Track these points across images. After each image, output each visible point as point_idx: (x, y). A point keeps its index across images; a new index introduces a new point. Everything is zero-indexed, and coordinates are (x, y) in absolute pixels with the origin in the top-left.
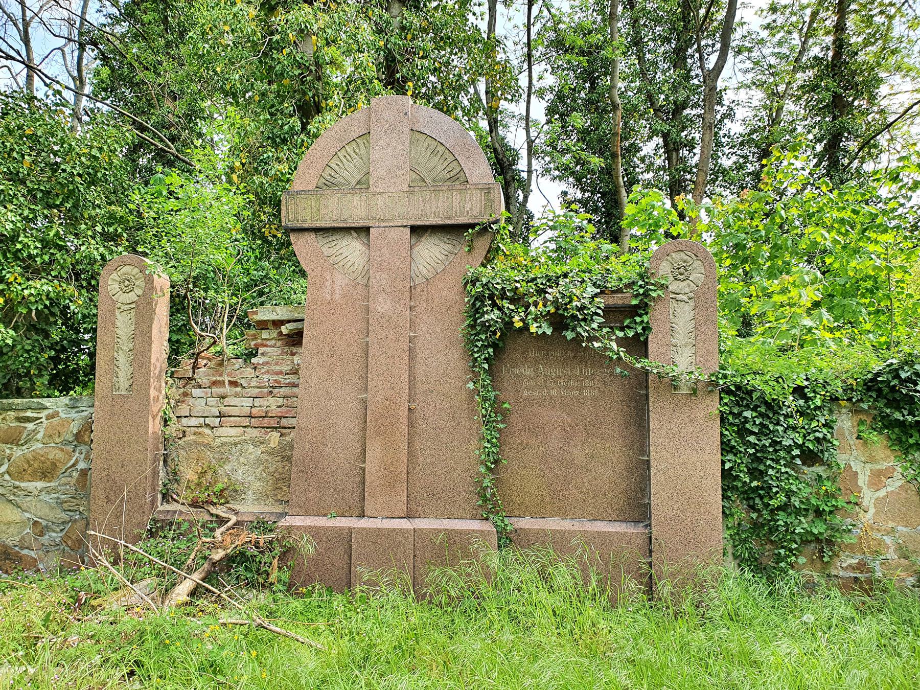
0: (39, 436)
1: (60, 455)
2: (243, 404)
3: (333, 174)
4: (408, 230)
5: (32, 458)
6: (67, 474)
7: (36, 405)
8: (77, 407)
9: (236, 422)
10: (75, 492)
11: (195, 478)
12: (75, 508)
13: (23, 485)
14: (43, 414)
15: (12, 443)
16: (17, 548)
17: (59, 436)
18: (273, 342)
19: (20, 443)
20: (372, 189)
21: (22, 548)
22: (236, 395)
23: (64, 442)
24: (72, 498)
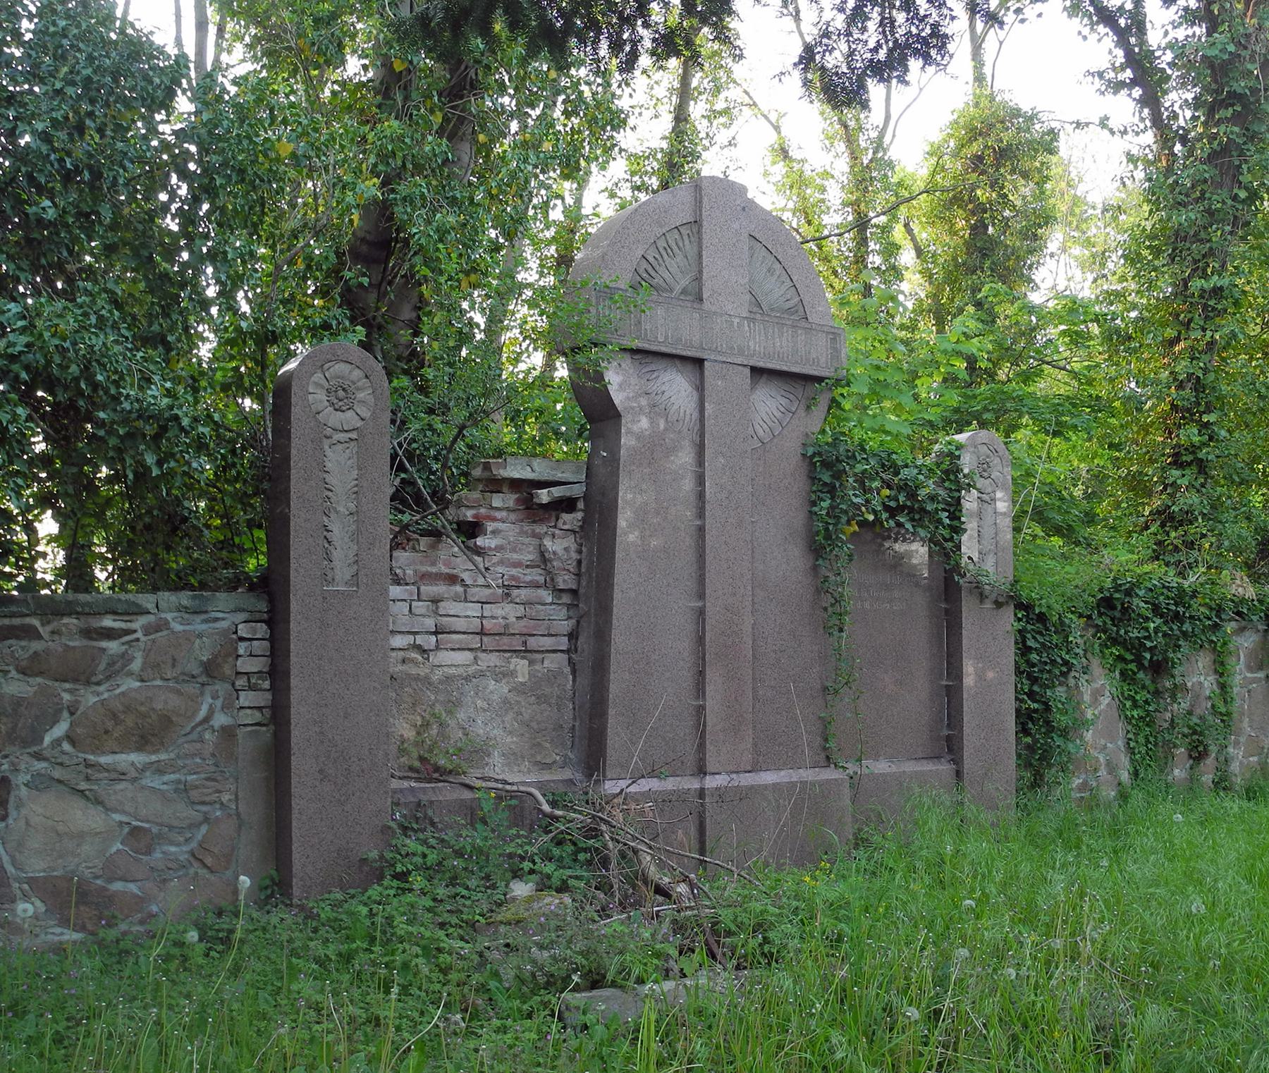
0: (136, 665)
1: (174, 702)
2: (469, 613)
3: (650, 270)
4: (748, 371)
5: (121, 708)
6: (194, 736)
7: (125, 606)
8: (206, 612)
9: (460, 641)
10: (213, 769)
11: (410, 734)
12: (214, 797)
13: (103, 760)
14: (139, 623)
15: (76, 680)
16: (99, 882)
17: (174, 666)
18: (504, 514)
19: (94, 679)
20: (707, 305)
21: (111, 880)
22: (456, 599)
23: (181, 678)
24: (207, 779)
